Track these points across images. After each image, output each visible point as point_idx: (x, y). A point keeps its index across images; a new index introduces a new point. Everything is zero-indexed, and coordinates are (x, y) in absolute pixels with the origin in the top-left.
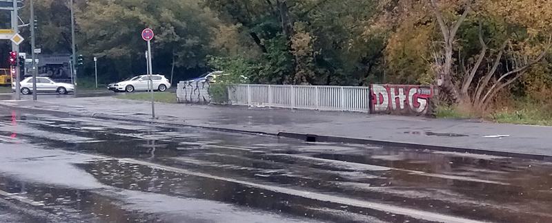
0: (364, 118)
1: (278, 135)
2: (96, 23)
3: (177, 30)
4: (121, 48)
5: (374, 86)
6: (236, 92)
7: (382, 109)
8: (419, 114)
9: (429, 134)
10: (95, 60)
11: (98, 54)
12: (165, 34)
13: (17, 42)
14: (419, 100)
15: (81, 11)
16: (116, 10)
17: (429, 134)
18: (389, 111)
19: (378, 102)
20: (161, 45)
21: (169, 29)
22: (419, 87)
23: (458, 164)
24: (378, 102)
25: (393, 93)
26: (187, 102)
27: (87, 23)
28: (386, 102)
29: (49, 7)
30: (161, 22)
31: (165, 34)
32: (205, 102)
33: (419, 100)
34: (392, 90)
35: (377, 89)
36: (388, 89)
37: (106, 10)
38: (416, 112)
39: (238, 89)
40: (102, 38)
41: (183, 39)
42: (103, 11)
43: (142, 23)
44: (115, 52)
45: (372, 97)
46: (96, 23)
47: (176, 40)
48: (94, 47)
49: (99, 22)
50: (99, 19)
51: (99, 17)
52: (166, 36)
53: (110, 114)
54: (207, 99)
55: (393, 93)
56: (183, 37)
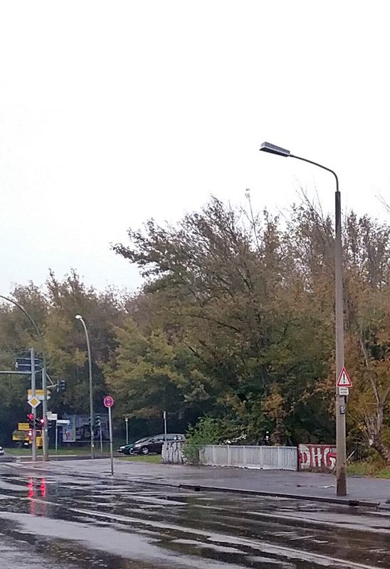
0: (295, 474)
1: (179, 487)
2: (126, 382)
3: (208, 388)
4: (151, 408)
5: (301, 445)
6: (205, 453)
7: (306, 468)
8: (330, 472)
9: (299, 486)
10: (127, 420)
11: (128, 415)
12: (194, 392)
13: (34, 405)
14: (331, 459)
15: (111, 370)
16: (145, 368)
17: (299, 486)
18: (310, 470)
19: (304, 461)
20: (191, 404)
21: (199, 387)
22: (331, 447)
23: (322, 511)
24: (304, 461)
25: (313, 453)
26: (170, 463)
27: (119, 382)
28: (309, 461)
29: (83, 366)
30: (191, 380)
31: (194, 392)
32: (183, 463)
33: (331, 459)
34: (313, 449)
35: (303, 448)
36: (309, 447)
37: (136, 367)
38: (328, 469)
39: (206, 449)
40: (132, 398)
41: (214, 397)
42: (132, 369)
43: (171, 381)
44: (144, 412)
45: (299, 457)
46: (126, 382)
47: (207, 398)
48: (126, 407)
49: (129, 381)
50: (128, 378)
51: (128, 376)
52: (195, 395)
53: (81, 472)
54: (185, 459)
55: (313, 453)
56: (214, 394)
